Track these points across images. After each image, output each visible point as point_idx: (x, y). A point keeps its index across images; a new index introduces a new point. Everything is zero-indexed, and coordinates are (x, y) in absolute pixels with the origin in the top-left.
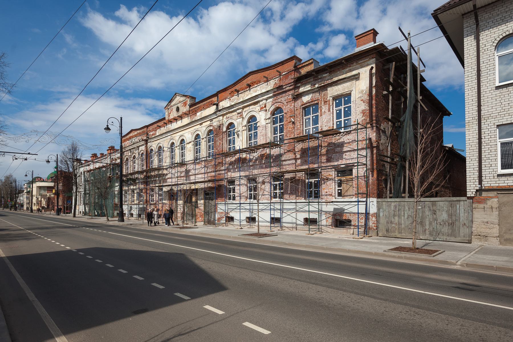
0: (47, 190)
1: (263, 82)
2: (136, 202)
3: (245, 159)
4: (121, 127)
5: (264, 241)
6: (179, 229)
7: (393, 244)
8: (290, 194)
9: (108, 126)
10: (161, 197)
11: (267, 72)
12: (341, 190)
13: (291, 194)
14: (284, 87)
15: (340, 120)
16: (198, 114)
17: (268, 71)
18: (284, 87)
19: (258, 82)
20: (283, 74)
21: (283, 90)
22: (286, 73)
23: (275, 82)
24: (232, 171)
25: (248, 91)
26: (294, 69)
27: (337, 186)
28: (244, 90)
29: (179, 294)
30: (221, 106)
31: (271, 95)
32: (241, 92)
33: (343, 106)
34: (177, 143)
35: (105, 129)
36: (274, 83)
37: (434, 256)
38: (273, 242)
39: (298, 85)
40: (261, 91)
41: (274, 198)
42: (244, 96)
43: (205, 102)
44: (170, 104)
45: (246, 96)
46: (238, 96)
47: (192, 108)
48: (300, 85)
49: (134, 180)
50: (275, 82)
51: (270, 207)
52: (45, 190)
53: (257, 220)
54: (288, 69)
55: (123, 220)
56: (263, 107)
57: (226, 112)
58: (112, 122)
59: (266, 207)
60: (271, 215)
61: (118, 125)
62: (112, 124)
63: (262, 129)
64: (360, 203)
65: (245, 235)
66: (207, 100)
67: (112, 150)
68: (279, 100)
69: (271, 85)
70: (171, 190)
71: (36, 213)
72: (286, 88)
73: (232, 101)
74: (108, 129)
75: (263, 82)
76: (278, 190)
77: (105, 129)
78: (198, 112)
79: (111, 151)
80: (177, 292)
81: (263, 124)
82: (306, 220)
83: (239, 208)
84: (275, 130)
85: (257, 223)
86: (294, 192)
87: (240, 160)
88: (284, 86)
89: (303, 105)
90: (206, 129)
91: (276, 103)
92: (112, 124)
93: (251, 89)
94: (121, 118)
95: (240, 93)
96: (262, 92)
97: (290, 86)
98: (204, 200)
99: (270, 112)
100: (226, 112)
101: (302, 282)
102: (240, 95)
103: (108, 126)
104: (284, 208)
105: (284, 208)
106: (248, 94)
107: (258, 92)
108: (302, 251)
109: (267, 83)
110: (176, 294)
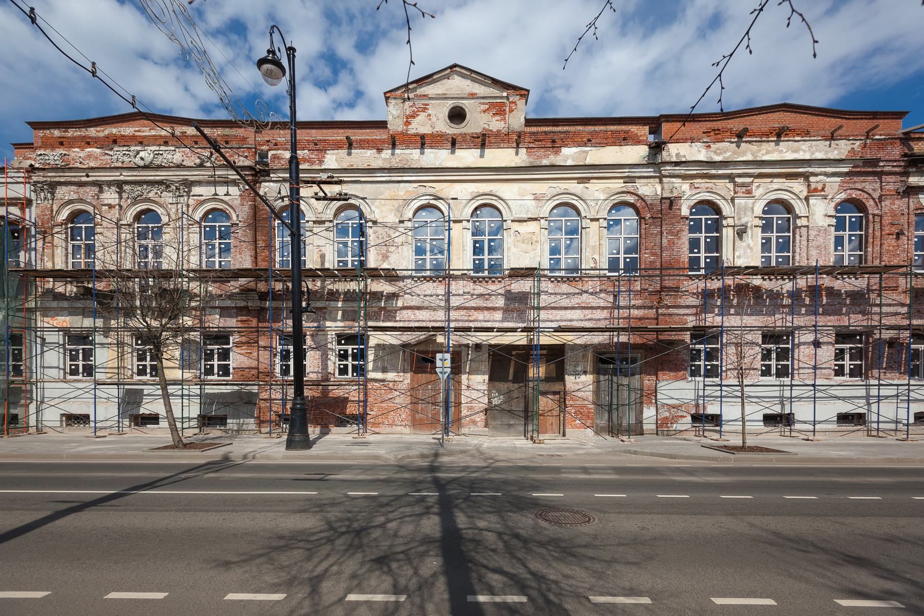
1: (819, 138)
2: (203, 376)
3: (757, 289)
8: (885, 369)
11: (828, 119)
13: (890, 368)
14: (881, 164)
15: (558, 256)
16: (565, 151)
17: (832, 119)
18: (881, 164)
19: (806, 133)
20: (877, 137)
21: (875, 169)
22: (883, 137)
23: (853, 146)
24: (716, 311)
25: (773, 144)
26: (902, 136)
27: (135, 359)
28: (763, 136)
30: (674, 155)
31: (846, 170)
32: (747, 139)
33: (487, 237)
36: (849, 148)
39: (911, 170)
40: (813, 154)
41: (71, 374)
42: (759, 151)
43: (597, 128)
44: (415, 89)
45: (764, 152)
46: (738, 146)
47: (528, 129)
48: (914, 170)
49: (129, 298)
50: (853, 146)
51: (93, 392)
53: (92, 418)
54: (890, 132)
56: (820, 188)
57: (698, 172)
59: (81, 392)
60: (908, 408)
63: (817, 233)
64: (794, 388)
65: (159, 448)
66: (606, 125)
68: (859, 186)
69: (841, 149)
70: (430, 341)
72: (884, 166)
73: (715, 152)
75: (819, 138)
78: (566, 146)
81: (820, 225)
82: (844, 418)
83: (180, 393)
84: (76, 249)
85: (92, 424)
86: (893, 366)
87: (741, 289)
88: (883, 161)
89: (917, 209)
90: (623, 192)
91: (851, 189)
93: (783, 141)
95: (746, 142)
96: (813, 157)
97: (893, 166)
98: (593, 373)
99: (833, 204)
100: (698, 172)
102: (781, 143)
104: (871, 394)
105: (871, 394)
106: (770, 149)
107: (801, 153)
109: (828, 142)
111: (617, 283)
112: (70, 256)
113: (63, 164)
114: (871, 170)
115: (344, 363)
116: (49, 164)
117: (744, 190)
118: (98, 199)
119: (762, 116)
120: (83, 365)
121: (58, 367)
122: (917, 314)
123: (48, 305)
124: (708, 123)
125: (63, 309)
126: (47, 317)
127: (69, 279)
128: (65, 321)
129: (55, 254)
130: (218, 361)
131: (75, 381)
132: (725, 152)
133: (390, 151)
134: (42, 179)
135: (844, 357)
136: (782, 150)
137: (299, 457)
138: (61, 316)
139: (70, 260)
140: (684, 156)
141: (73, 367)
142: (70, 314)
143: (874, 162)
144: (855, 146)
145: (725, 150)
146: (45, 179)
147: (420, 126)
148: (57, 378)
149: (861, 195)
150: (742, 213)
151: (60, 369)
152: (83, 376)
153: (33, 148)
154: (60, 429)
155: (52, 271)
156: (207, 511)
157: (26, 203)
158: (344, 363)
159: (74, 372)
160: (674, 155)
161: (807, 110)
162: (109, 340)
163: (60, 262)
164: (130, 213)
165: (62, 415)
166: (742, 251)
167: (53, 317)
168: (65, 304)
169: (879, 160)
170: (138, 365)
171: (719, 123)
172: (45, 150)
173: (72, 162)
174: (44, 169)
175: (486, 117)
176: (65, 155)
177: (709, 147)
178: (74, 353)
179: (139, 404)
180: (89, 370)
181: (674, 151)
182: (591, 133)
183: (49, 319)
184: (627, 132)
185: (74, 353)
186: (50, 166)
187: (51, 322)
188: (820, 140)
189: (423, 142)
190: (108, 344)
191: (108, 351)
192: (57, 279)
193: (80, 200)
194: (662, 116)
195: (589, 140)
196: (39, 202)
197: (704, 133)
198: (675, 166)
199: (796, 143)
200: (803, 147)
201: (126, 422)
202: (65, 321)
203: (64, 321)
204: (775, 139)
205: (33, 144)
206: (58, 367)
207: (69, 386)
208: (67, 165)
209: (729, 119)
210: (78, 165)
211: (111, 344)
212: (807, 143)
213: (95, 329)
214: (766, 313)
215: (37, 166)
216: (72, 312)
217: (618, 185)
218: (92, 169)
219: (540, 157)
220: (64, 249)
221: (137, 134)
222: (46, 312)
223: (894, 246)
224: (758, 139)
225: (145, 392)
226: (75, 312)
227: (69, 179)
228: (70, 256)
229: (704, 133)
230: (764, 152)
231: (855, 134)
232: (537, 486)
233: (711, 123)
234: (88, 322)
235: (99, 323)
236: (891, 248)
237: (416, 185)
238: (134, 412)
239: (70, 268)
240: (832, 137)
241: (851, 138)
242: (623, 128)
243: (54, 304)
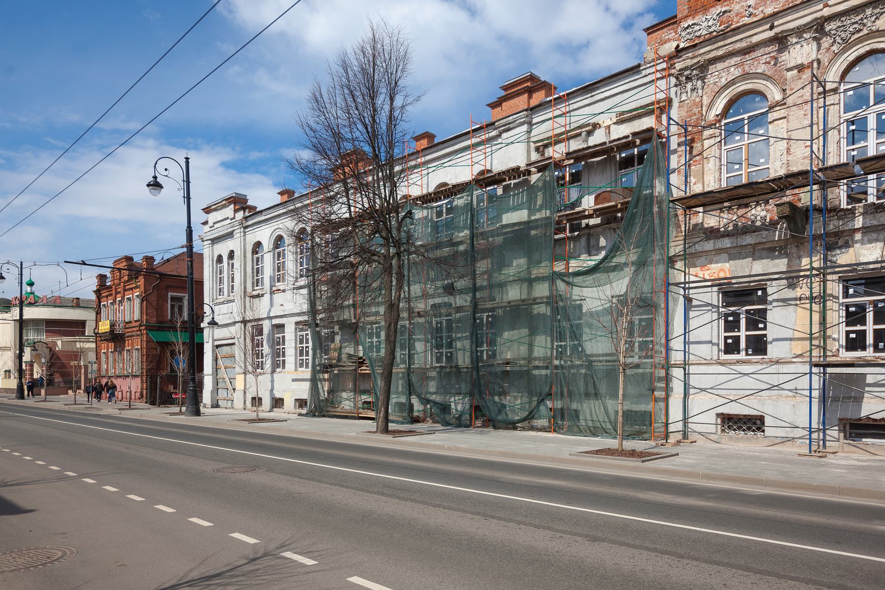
0: (47, 331)
4: (188, 182)
5: (402, 443)
6: (168, 416)
7: (588, 444)
9: (155, 177)
10: (260, 360)
12: (451, 353)
29: (309, 564)
34: (267, 245)
35: (148, 185)
37: (643, 461)
38: (421, 445)
52: (38, 331)
55: (197, 413)
58: (166, 170)
61: (16, 271)
62: (8, 271)
65: (587, 452)
67: (247, 210)
71: (181, 413)
74: (155, 185)
76: (485, 345)
77: (148, 185)
79: (244, 212)
80: (351, 576)
92: (8, 271)
94: (21, 262)
101: (570, 536)
103: (155, 177)
108: (567, 471)
110: (191, 519)
111: (323, 293)
112: (724, 169)
113: (722, 27)
115: (859, 328)
116: (699, 37)
118: (775, 65)
120: (875, 330)
121: (710, 342)
123: (698, 247)
125: (719, 251)
126: (695, 266)
127: (726, 204)
128: (722, 270)
129: (706, 170)
130: (747, 330)
131: (738, 362)
134: (689, 62)
135: (864, 317)
137: (20, 402)
138: (717, 262)
139: (724, 175)
141: (730, 341)
142: (732, 258)
146: (695, 61)
148: (708, 358)
151: (713, 344)
152: (747, 354)
153: (675, 23)
154: (713, 437)
155: (788, 176)
156: (321, 482)
157: (663, 107)
158: (859, 328)
159: (732, 347)
162: (798, 292)
163: (712, 181)
164: (835, 69)
165: (296, 400)
167: (703, 266)
168: (727, 243)
170: (726, 338)
172: (694, 18)
173: (735, 19)
174: (694, 46)
176: (725, 12)
178: (731, 318)
179: (858, 400)
180: (759, 346)
183: (698, 269)
185: (731, 318)
186: (701, 39)
187: (701, 274)
190: (795, 299)
191: (796, 312)
192: (708, 208)
193: (746, 76)
196: (684, 97)
201: (833, 432)
202: (722, 270)
203: (722, 269)
205: (676, 17)
206: (710, 342)
207: (728, 371)
208: (727, 27)
210: (747, 20)
211: (800, 299)
213: (769, 277)
216: (735, 254)
218: (775, 15)
220: (717, 160)
222: (690, 258)
225: (870, 379)
226: (740, 253)
227: (730, 48)
228: (724, 169)
234: (759, 267)
235: (781, 265)
238: (850, 415)
239: (724, 185)
243: (709, 245)
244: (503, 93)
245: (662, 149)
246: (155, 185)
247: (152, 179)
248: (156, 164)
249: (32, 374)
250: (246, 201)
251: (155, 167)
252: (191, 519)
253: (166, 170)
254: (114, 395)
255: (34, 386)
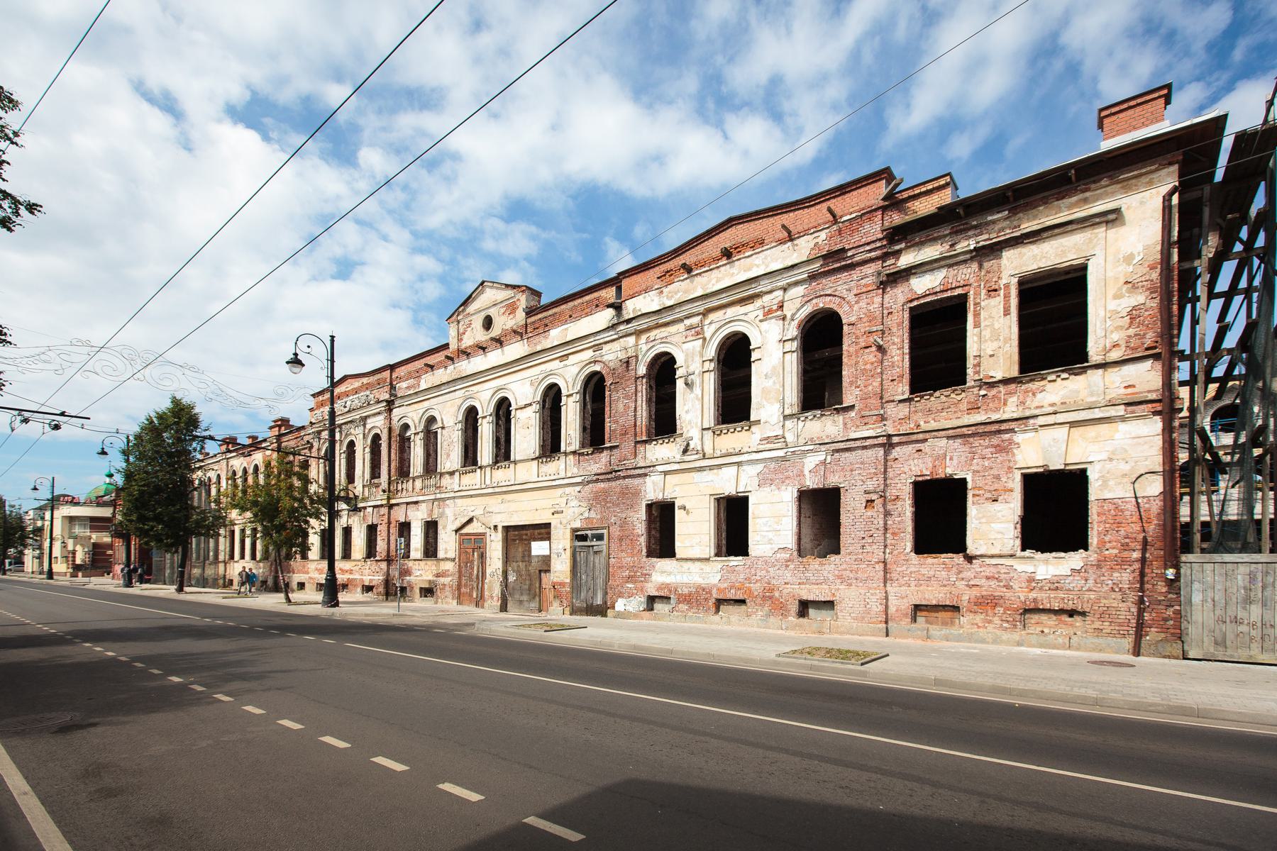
1: (775, 244)
4: (332, 361)
9: (296, 354)
17: (791, 214)
18: (850, 254)
19: (758, 244)
22: (854, 215)
23: (816, 241)
29: (399, 770)
30: (631, 311)
36: (812, 245)
37: (862, 664)
39: (897, 247)
40: (767, 266)
42: (710, 281)
45: (714, 281)
48: (903, 245)
50: (816, 241)
58: (309, 347)
61: (323, 354)
62: (308, 350)
73: (668, 298)
74: (296, 362)
92: (308, 350)
97: (870, 251)
106: (720, 276)
110: (441, 786)
114: (838, 265)
117: (693, 332)
119: (713, 239)
122: (916, 455)
124: (661, 266)
132: (676, 294)
133: (452, 367)
136: (733, 273)
140: (640, 310)
143: (839, 253)
144: (819, 240)
145: (682, 289)
147: (468, 342)
149: (830, 301)
150: (690, 360)
160: (631, 311)
161: (751, 216)
166: (690, 405)
169: (843, 250)
171: (671, 262)
175: (504, 318)
177: (662, 292)
181: (633, 307)
182: (571, 309)
184: (597, 299)
188: (776, 246)
189: (465, 353)
194: (620, 274)
195: (570, 316)
197: (658, 278)
198: (627, 324)
199: (748, 259)
200: (757, 262)
204: (686, 276)
209: (680, 254)
212: (761, 254)
214: (40, 536)
215: (314, 422)
217: (588, 355)
219: (536, 344)
221: (347, 389)
223: (872, 364)
224: (707, 268)
229: (658, 278)
230: (714, 281)
231: (815, 224)
232: (435, 628)
233: (664, 265)
236: (868, 367)
237: (463, 391)
240: (791, 237)
241: (812, 231)
242: (596, 295)
244: (273, 424)
245: (93, 519)
246: (296, 362)
247: (293, 356)
248: (297, 340)
249: (74, 561)
250: (236, 439)
251: (296, 343)
252: (441, 786)
253: (309, 347)
254: (1233, 632)
255: (77, 568)
